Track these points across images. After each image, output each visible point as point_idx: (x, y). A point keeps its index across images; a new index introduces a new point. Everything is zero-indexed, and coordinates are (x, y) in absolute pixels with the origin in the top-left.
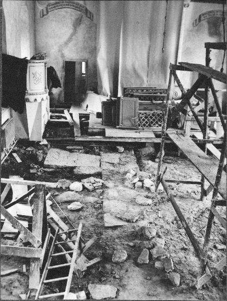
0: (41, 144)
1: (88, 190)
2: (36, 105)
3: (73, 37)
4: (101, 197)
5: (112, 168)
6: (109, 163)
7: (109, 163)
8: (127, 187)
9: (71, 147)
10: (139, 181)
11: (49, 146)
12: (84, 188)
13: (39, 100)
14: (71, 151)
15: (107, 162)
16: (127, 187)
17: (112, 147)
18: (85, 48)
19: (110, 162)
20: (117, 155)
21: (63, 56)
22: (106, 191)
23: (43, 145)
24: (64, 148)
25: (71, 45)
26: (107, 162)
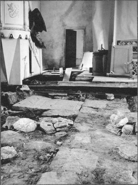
0: (21, 89)
1: (44, 132)
2: (13, 43)
3: (73, 8)
4: (58, 143)
5: (93, 112)
6: (92, 107)
7: (92, 107)
8: (109, 132)
9: (53, 94)
10: (128, 124)
11: (31, 93)
12: (38, 128)
13: (16, 36)
14: (53, 97)
15: (90, 107)
16: (109, 132)
17: (100, 93)
18: (83, 16)
19: (94, 107)
20: (105, 101)
21: (64, 25)
22: (72, 136)
23: (25, 91)
24: (47, 96)
25: (70, 14)
26: (90, 107)
